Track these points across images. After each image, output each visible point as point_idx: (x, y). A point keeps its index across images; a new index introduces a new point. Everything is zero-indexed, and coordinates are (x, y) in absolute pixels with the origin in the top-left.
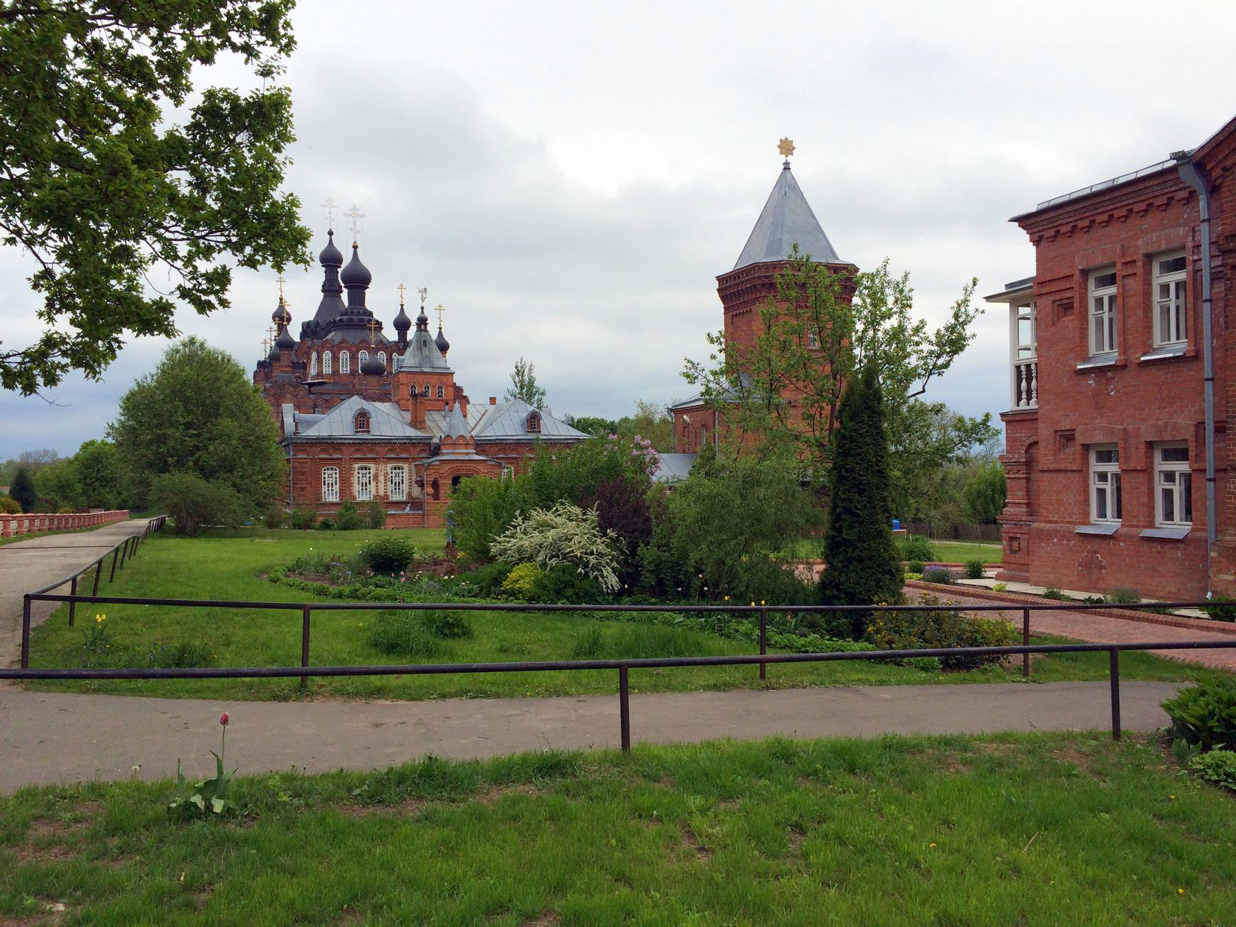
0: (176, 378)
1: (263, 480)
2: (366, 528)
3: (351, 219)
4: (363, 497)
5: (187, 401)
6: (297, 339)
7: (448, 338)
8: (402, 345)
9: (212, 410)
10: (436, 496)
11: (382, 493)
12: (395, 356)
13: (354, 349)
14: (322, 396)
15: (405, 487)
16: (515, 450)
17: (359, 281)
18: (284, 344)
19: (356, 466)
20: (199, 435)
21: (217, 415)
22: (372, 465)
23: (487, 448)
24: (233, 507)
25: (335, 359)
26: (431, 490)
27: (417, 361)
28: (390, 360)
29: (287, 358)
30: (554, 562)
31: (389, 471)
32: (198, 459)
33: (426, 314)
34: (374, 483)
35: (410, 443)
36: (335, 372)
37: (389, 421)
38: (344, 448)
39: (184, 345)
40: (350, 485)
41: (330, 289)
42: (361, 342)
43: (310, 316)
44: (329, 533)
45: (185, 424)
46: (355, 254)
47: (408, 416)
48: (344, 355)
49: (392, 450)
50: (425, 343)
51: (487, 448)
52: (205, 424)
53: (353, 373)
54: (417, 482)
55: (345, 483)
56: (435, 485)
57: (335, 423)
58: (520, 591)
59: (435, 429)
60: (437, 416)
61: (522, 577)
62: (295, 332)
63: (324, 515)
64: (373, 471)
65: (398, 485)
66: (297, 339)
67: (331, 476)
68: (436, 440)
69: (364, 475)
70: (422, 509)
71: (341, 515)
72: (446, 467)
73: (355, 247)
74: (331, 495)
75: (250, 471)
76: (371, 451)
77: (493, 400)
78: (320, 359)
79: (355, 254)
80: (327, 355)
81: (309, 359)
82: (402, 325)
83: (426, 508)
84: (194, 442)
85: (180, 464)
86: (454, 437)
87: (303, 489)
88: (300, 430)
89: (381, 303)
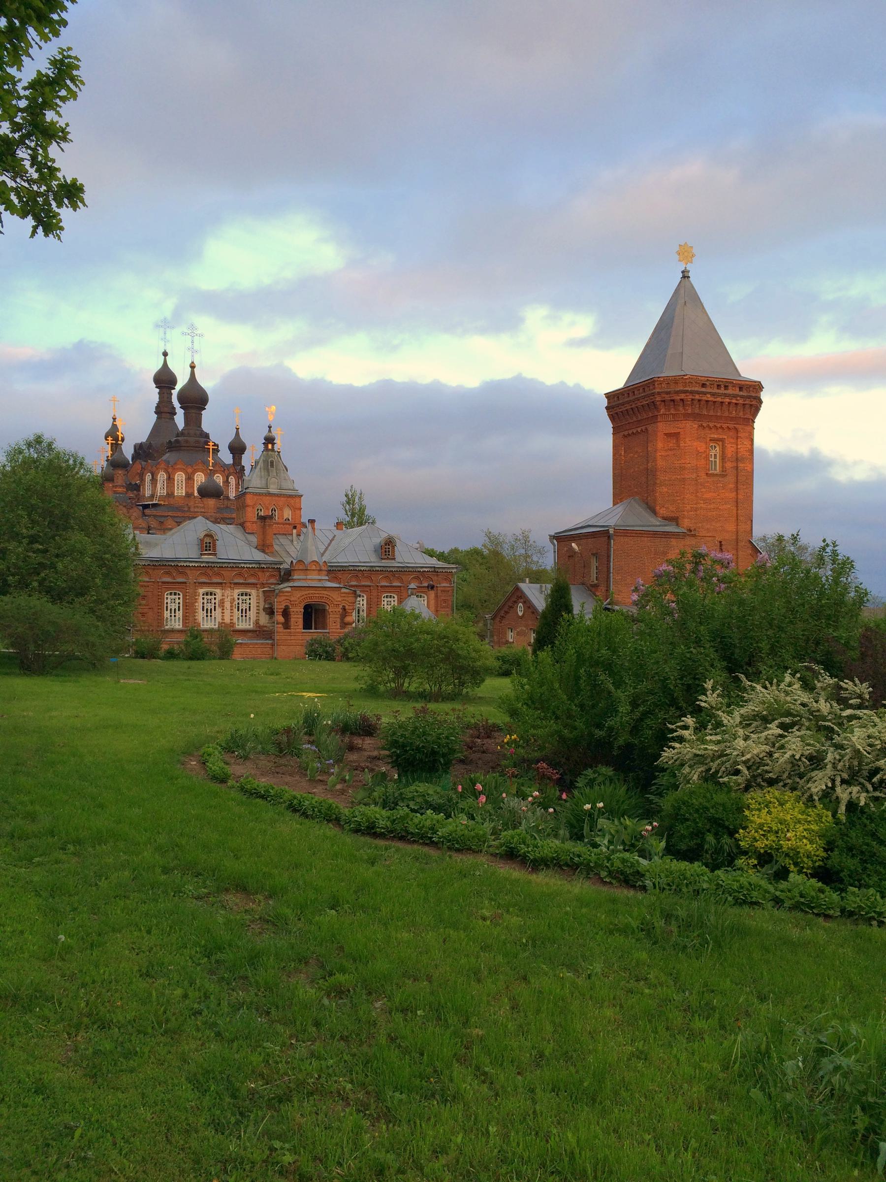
0: (19, 482)
4: (207, 624)
6: (129, 456)
10: (286, 625)
14: (162, 515)
15: (252, 614)
19: (201, 591)
20: (45, 551)
22: (218, 591)
25: (170, 479)
26: (281, 619)
27: (264, 482)
29: (120, 476)
31: (236, 597)
32: (44, 579)
33: (274, 433)
34: (228, 609)
35: (260, 567)
37: (235, 545)
39: (29, 445)
40: (194, 612)
41: (164, 410)
45: (28, 537)
47: (254, 539)
48: (180, 477)
49: (240, 575)
50: (272, 462)
51: (339, 575)
52: (53, 537)
53: (189, 495)
55: (189, 609)
56: (286, 613)
57: (177, 544)
59: (283, 554)
60: (283, 540)
61: (786, 822)
62: (128, 451)
63: (170, 643)
64: (219, 597)
65: (244, 612)
66: (129, 456)
67: (173, 602)
68: (285, 566)
70: (271, 638)
71: (187, 644)
72: (298, 594)
73: (193, 367)
75: (105, 596)
76: (219, 575)
78: (154, 481)
79: (193, 374)
80: (162, 476)
81: (142, 480)
83: (277, 637)
84: (40, 558)
85: (23, 585)
87: (143, 615)
89: (216, 423)
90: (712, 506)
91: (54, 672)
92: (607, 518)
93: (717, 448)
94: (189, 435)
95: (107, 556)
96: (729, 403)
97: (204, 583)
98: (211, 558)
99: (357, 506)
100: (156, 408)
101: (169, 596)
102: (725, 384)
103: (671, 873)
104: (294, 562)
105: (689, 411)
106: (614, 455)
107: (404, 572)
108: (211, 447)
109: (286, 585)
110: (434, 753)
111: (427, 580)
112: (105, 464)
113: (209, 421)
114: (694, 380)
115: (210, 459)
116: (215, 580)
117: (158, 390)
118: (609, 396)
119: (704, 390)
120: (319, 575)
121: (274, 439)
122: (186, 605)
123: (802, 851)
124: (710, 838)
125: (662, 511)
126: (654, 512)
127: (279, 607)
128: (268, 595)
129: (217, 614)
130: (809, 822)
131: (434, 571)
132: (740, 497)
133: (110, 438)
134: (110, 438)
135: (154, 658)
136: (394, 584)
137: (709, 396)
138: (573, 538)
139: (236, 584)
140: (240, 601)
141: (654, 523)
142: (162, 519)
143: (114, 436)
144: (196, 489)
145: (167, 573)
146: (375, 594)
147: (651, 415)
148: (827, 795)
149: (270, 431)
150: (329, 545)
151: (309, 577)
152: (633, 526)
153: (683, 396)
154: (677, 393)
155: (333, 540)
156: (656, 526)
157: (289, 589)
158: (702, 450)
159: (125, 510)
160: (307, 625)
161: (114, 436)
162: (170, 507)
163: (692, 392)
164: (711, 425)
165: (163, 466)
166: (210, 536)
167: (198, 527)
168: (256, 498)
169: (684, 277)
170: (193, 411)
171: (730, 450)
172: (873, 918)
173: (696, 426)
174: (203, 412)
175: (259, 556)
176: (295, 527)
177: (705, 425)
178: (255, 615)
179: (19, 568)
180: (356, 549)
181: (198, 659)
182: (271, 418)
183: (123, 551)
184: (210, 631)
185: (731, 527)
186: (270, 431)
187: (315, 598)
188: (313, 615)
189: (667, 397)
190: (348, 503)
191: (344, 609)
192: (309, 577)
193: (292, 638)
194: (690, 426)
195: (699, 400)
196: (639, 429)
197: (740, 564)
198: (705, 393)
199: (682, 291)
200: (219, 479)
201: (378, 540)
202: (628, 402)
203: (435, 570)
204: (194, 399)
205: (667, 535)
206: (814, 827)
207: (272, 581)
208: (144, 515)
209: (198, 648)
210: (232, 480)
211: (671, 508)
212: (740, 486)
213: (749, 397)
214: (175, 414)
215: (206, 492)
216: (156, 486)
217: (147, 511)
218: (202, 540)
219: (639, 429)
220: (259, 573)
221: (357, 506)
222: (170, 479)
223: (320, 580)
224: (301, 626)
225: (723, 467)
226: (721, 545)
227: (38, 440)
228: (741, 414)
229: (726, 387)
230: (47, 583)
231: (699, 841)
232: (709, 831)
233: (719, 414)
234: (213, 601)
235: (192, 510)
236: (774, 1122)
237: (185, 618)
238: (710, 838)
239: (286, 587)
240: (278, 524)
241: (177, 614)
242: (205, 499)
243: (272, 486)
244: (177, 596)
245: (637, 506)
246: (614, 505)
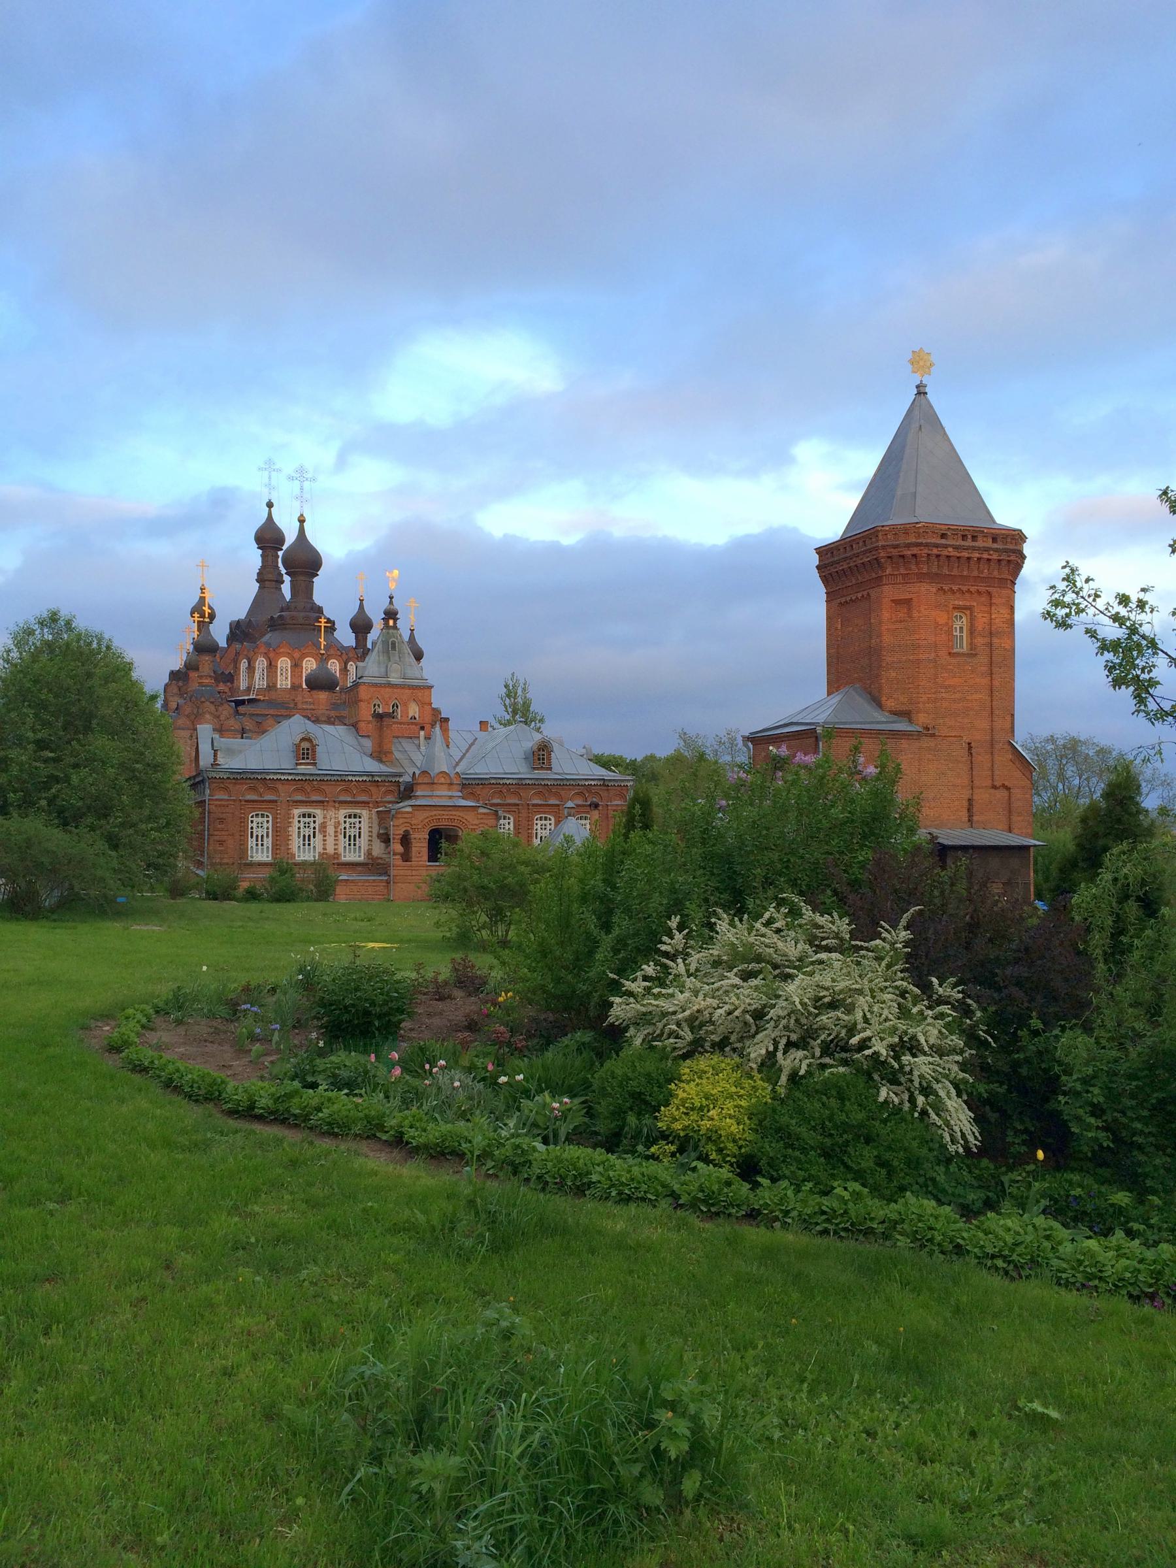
1: (158, 830)
2: (308, 899)
4: (304, 855)
5: (43, 706)
6: (223, 643)
7: (421, 643)
8: (361, 651)
9: (81, 722)
10: (406, 857)
11: (330, 850)
12: (351, 666)
14: (252, 714)
15: (363, 842)
18: (204, 647)
19: (296, 812)
20: (55, 760)
21: (88, 729)
22: (318, 812)
24: (99, 873)
26: (399, 848)
27: (383, 670)
28: (344, 670)
30: (794, 1061)
31: (342, 819)
32: (55, 797)
33: (397, 605)
34: (329, 836)
35: (374, 781)
37: (342, 751)
38: (279, 786)
39: (42, 623)
40: (287, 838)
41: (267, 578)
43: (240, 612)
44: (254, 906)
47: (368, 744)
48: (284, 663)
49: (347, 791)
50: (393, 644)
51: (478, 790)
52: (69, 742)
53: (295, 687)
55: (280, 835)
57: (268, 752)
58: (713, 1137)
59: (405, 763)
60: (407, 745)
61: (715, 1098)
62: (220, 633)
66: (223, 643)
67: (260, 825)
70: (386, 873)
71: (272, 880)
72: (422, 816)
76: (318, 790)
77: (483, 725)
78: (251, 669)
79: (302, 530)
80: (261, 663)
81: (237, 668)
82: (361, 626)
83: (393, 872)
84: (51, 769)
85: (27, 804)
87: (221, 843)
88: (220, 760)
89: (333, 596)
90: (957, 696)
91: (55, 917)
92: (817, 712)
93: (964, 619)
95: (137, 766)
96: (979, 559)
97: (345, 802)
98: (310, 769)
99: (519, 700)
100: (258, 574)
101: (254, 819)
102: (974, 534)
103: (561, 1161)
104: (417, 772)
105: (925, 570)
106: (828, 629)
107: (563, 786)
108: (323, 625)
109: (406, 803)
110: (367, 1013)
111: (589, 797)
112: (191, 648)
113: (323, 591)
114: (929, 529)
115: (322, 640)
116: (314, 798)
118: (819, 551)
119: (943, 541)
120: (449, 790)
121: (396, 613)
122: (276, 830)
123: (723, 1133)
124: (632, 1119)
125: (890, 704)
126: (880, 705)
127: (396, 832)
128: (383, 817)
129: (317, 841)
130: (741, 1096)
131: (604, 785)
132: (996, 683)
133: (196, 615)
134: (196, 615)
135: (230, 899)
136: (551, 802)
137: (950, 549)
138: (776, 739)
139: (341, 802)
140: (348, 825)
141: (879, 719)
142: (259, 719)
143: (203, 614)
145: (297, 789)
147: (874, 575)
148: (769, 1064)
149: (391, 603)
150: (467, 751)
151: (435, 793)
152: (845, 723)
153: (915, 550)
154: (908, 546)
155: (473, 744)
156: (883, 722)
157: (409, 809)
158: (942, 621)
159: (212, 708)
160: (433, 855)
161: (203, 614)
162: (271, 703)
163: (927, 545)
164: (955, 588)
165: (263, 650)
166: (309, 740)
167: (294, 727)
168: (372, 689)
169: (919, 393)
170: (302, 578)
171: (981, 621)
172: (776, 1219)
173: (934, 590)
175: (372, 766)
176: (422, 728)
177: (946, 588)
179: (24, 782)
180: (504, 756)
181: (288, 901)
182: (393, 586)
183: (159, 759)
184: (304, 864)
185: (984, 724)
186: (391, 603)
187: (443, 821)
188: (439, 840)
189: (895, 552)
190: (508, 696)
192: (435, 793)
193: (414, 873)
194: (925, 591)
195: (938, 556)
196: (859, 595)
197: (997, 772)
198: (946, 546)
199: (916, 412)
200: (334, 666)
202: (845, 559)
203: (604, 783)
204: (306, 563)
205: (895, 734)
206: (743, 1103)
207: (389, 798)
208: (237, 712)
209: (288, 886)
211: (901, 699)
212: (995, 670)
213: (1006, 551)
214: (283, 582)
215: (319, 683)
216: (253, 677)
217: (241, 709)
218: (298, 746)
219: (859, 595)
220: (231, 786)
221: (519, 700)
222: (271, 666)
223: (451, 797)
224: (426, 858)
225: (971, 644)
226: (970, 748)
227: (54, 617)
228: (996, 573)
229: (974, 538)
230: (59, 802)
231: (620, 1123)
232: (631, 1109)
233: (965, 573)
234: (312, 825)
235: (300, 706)
237: (276, 847)
238: (632, 1119)
239: (406, 806)
240: (401, 723)
242: (314, 692)
243: (393, 675)
244: (548, 822)
245: (857, 697)
246: (829, 694)
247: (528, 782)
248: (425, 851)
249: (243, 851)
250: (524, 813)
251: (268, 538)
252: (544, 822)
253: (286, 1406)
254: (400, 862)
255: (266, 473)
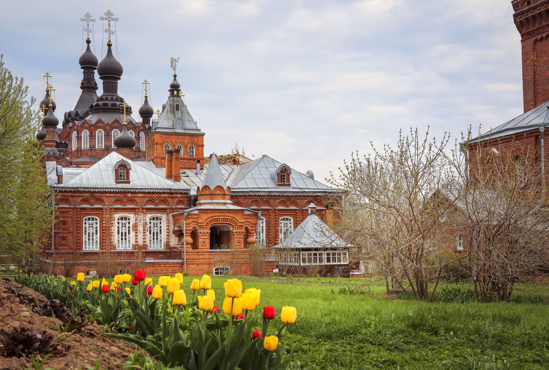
3: (106, 22)
10: (195, 245)
11: (140, 243)
13: (108, 128)
15: (163, 236)
16: (267, 203)
17: (112, 73)
19: (117, 216)
22: (132, 216)
23: (241, 200)
25: (92, 136)
26: (190, 240)
31: (148, 221)
33: (179, 81)
36: (92, 148)
37: (147, 175)
40: (110, 235)
41: (88, 86)
42: (113, 123)
43: (71, 107)
46: (110, 51)
48: (100, 133)
49: (151, 201)
50: (177, 106)
54: (174, 232)
56: (194, 235)
57: (98, 174)
64: (132, 221)
65: (156, 236)
67: (91, 228)
68: (193, 193)
69: (124, 225)
72: (204, 217)
73: (109, 45)
74: (91, 244)
78: (79, 138)
80: (85, 134)
86: (212, 188)
94: (107, 99)
100: (82, 84)
101: (87, 222)
117: (83, 70)
120: (224, 199)
133: (44, 106)
136: (291, 208)
138: (494, 143)
139: (149, 210)
140: (152, 225)
144: (113, 142)
146: (273, 217)
149: (175, 80)
151: (214, 201)
157: (197, 212)
174: (119, 82)
176: (199, 162)
178: (166, 237)
186: (175, 80)
191: (247, 229)
193: (201, 257)
201: (274, 170)
210: (142, 135)
223: (225, 204)
224: (208, 246)
234: (127, 225)
236: (149, 323)
239: (194, 210)
241: (95, 238)
244: (289, 222)
246: (525, 111)
247: (275, 194)
248: (208, 241)
249: (79, 244)
250: (272, 215)
251: (88, 63)
252: (286, 222)
253: (27, 314)
254: (191, 250)
255: (86, 22)
